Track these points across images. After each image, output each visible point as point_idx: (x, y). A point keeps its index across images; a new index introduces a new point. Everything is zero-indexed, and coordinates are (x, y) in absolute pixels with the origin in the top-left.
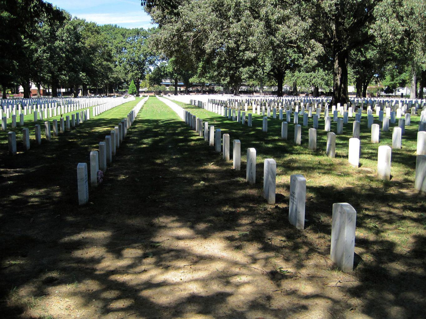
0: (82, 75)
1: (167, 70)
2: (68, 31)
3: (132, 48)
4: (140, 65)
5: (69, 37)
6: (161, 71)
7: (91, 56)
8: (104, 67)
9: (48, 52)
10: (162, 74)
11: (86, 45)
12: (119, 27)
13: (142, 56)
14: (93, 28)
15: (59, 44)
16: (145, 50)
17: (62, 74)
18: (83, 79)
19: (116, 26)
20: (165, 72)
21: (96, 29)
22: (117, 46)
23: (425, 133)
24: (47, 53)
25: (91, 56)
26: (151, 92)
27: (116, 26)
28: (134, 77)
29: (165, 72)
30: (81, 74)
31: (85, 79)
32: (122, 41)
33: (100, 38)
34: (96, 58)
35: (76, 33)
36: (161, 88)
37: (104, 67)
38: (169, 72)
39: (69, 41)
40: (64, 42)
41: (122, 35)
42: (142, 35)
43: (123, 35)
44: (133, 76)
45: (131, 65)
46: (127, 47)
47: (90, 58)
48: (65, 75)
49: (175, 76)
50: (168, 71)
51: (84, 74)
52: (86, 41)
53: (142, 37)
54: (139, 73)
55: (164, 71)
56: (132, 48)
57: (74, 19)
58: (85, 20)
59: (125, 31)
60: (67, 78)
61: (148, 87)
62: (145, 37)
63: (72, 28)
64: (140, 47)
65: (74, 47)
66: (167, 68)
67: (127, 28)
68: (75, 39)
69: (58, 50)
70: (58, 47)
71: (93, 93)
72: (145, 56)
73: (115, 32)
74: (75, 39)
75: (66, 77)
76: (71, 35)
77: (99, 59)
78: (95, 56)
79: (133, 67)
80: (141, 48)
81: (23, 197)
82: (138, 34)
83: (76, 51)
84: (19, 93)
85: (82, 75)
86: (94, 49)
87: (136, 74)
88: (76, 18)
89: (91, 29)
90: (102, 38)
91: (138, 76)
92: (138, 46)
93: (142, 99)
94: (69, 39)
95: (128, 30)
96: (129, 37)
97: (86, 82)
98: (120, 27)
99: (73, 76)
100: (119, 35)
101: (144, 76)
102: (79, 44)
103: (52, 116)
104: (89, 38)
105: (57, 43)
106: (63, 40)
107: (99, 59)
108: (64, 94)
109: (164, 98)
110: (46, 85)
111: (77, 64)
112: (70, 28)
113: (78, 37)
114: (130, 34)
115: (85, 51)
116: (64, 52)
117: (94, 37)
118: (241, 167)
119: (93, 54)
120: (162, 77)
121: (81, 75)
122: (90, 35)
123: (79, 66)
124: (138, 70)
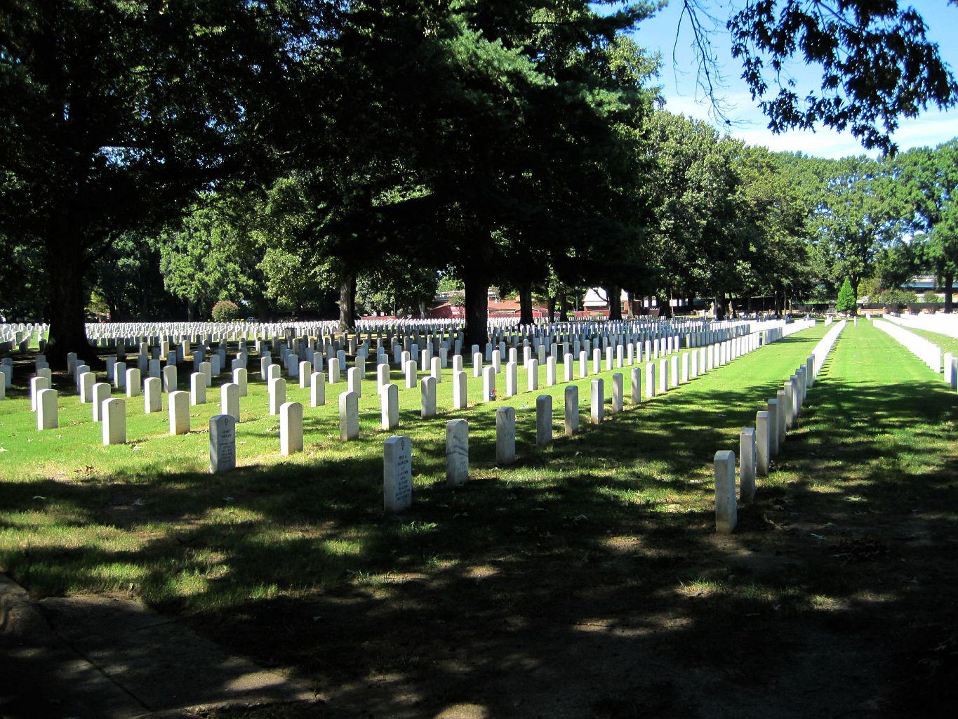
0: (744, 268)
1: (928, 254)
2: (712, 167)
3: (841, 202)
4: (862, 242)
5: (714, 181)
6: (914, 256)
7: (758, 223)
8: (788, 249)
9: (670, 216)
10: (917, 261)
11: (748, 199)
12: (806, 156)
13: (865, 222)
14: (760, 160)
15: (692, 197)
16: (876, 208)
17: (695, 266)
18: (744, 276)
19: (799, 154)
20: (925, 258)
21: (768, 162)
22: (806, 201)
23: (210, 469)
24: (668, 218)
25: (758, 223)
26: (879, 306)
27: (799, 154)
28: (848, 272)
29: (925, 258)
30: (739, 264)
31: (749, 277)
32: (818, 189)
33: (779, 180)
34: (771, 227)
35: (729, 172)
36: (903, 296)
37: (788, 249)
38: (934, 257)
39: (714, 189)
40: (702, 194)
41: (815, 173)
42: (866, 172)
43: (817, 174)
44: (845, 268)
45: (840, 244)
46: (829, 200)
47: (758, 227)
48: (701, 267)
49: (949, 266)
50: (932, 254)
51: (748, 265)
52: (748, 190)
53: (864, 177)
54: (860, 261)
55: (923, 255)
56: (841, 202)
57: (723, 140)
58: (744, 142)
59: (823, 164)
60: (709, 274)
61: (870, 294)
62: (870, 176)
63: (722, 160)
64: (861, 199)
65: (726, 202)
66: (929, 247)
67: (828, 157)
68: (726, 185)
69: (691, 210)
70: (691, 203)
71: (741, 309)
72: (875, 220)
73: (798, 168)
74: (726, 185)
75: (706, 272)
76: (718, 176)
77: (778, 230)
78: (767, 223)
79: (845, 248)
80: (865, 201)
81: (345, 535)
82: (854, 168)
83: (725, 211)
84: (583, 310)
85: (743, 266)
86: (762, 206)
87: (854, 264)
88: (729, 138)
89: (757, 162)
90: (784, 181)
91: (858, 269)
92: (855, 197)
93: (829, 327)
94: (715, 185)
95: (830, 162)
96: (834, 177)
97: (752, 282)
98: (809, 157)
99: (722, 269)
100: (809, 174)
101: (873, 268)
102: (736, 196)
103: (599, 371)
104: (754, 183)
105: (687, 197)
106: (699, 189)
107: (778, 230)
108: (678, 310)
109: (887, 320)
110: (663, 291)
111: (731, 242)
112: (717, 160)
113: (732, 181)
114: (837, 170)
115: (744, 214)
116: (703, 216)
117: (766, 179)
118: (739, 512)
119: (763, 219)
120: (915, 270)
121: (739, 268)
122: (757, 175)
123: (736, 246)
124: (856, 256)
